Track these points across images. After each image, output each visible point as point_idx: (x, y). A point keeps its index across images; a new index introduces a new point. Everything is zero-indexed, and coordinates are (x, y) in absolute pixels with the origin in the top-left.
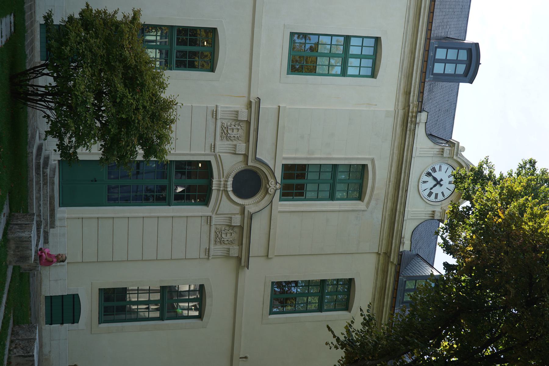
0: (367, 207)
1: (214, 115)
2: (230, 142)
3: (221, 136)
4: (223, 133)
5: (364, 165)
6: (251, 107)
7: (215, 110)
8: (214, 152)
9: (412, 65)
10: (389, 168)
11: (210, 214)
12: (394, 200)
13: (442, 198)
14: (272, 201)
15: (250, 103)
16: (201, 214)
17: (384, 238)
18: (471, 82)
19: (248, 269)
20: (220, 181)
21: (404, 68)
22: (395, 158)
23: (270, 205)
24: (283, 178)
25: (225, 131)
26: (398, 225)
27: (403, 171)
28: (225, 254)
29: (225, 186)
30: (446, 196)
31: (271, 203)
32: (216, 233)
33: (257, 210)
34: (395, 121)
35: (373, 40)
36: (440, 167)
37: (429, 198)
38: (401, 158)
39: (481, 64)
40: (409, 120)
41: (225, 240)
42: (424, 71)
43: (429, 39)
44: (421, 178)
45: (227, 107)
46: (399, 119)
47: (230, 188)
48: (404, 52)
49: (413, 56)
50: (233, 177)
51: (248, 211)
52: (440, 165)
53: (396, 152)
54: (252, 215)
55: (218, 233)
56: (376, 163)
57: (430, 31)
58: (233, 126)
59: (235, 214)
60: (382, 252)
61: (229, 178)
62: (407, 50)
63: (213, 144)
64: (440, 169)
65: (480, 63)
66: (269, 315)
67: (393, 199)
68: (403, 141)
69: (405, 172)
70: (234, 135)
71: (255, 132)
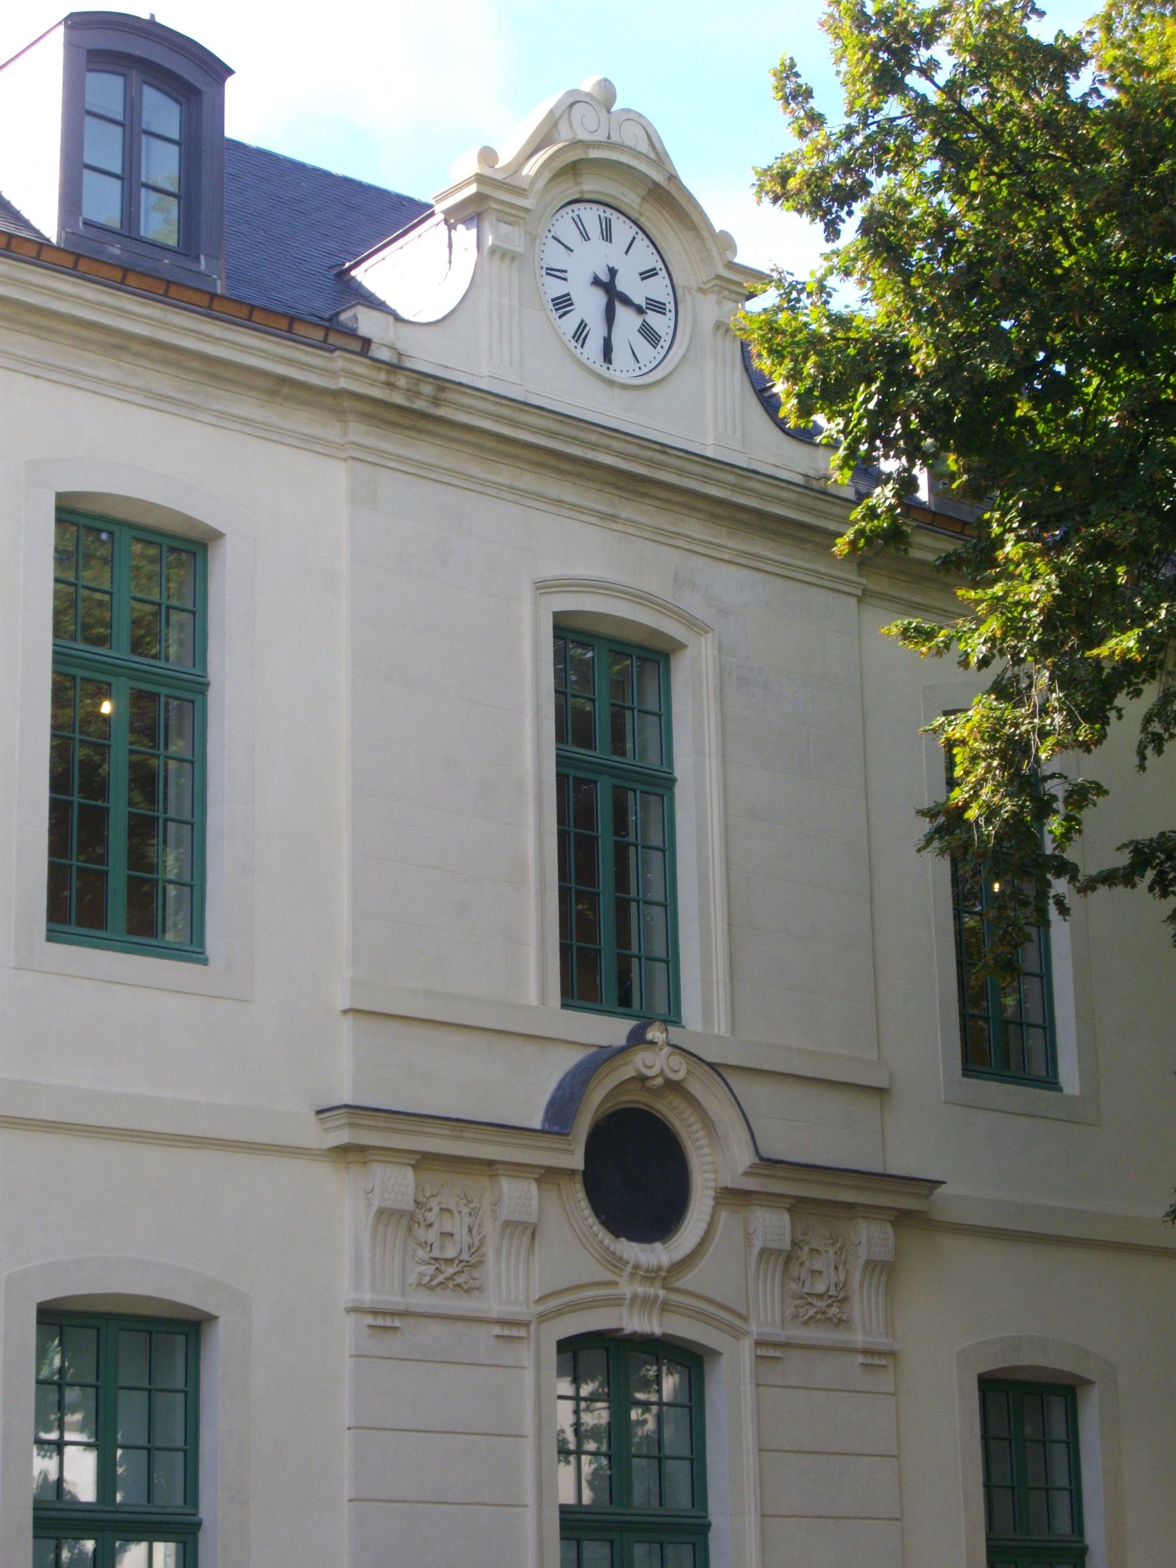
0: (706, 629)
1: (388, 1322)
2: (490, 1250)
3: (468, 1291)
4: (459, 1280)
5: (59, 510)
6: (363, 1149)
7: (370, 1320)
8: (527, 1324)
9: (171, 356)
10: (565, 512)
11: (746, 1346)
12: (679, 504)
13: (661, 280)
14: (712, 1066)
15: (345, 1153)
16: (747, 1390)
17: (812, 566)
18: (219, 71)
19: (944, 1183)
20: (635, 1297)
21: (183, 397)
22: (529, 480)
23: (722, 1071)
24: (598, 1006)
25: (450, 1270)
26: (781, 501)
27: (590, 455)
28: (883, 1279)
29: (650, 1275)
30: (653, 261)
31: (721, 1070)
32: (811, 1318)
33: (742, 1133)
34: (391, 464)
35: (170, 294)
36: (551, 272)
37: (662, 343)
38: (535, 456)
39: (152, 16)
40: (398, 398)
41: (833, 1278)
42: (205, 300)
43: (211, 301)
44: (590, 364)
45: (357, 1261)
46: (383, 445)
47: (657, 1255)
48: (116, 384)
49: (135, 346)
50: (613, 1238)
51: (746, 1174)
52: (543, 272)
53: (505, 474)
54: (762, 1159)
55: (811, 1312)
56: (551, 570)
57: (45, 250)
58: (432, 1236)
59: (748, 1236)
60: (854, 577)
61: (625, 1256)
62: (106, 368)
63: (497, 1330)
64: (554, 273)
65: (147, 17)
66: (1060, 1090)
67: (675, 508)
68: (472, 438)
69: (595, 447)
70: (466, 1230)
71: (466, 1134)
